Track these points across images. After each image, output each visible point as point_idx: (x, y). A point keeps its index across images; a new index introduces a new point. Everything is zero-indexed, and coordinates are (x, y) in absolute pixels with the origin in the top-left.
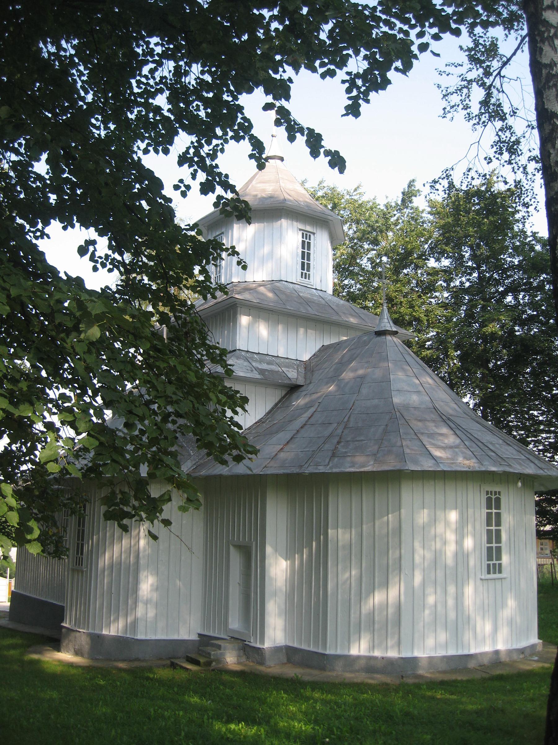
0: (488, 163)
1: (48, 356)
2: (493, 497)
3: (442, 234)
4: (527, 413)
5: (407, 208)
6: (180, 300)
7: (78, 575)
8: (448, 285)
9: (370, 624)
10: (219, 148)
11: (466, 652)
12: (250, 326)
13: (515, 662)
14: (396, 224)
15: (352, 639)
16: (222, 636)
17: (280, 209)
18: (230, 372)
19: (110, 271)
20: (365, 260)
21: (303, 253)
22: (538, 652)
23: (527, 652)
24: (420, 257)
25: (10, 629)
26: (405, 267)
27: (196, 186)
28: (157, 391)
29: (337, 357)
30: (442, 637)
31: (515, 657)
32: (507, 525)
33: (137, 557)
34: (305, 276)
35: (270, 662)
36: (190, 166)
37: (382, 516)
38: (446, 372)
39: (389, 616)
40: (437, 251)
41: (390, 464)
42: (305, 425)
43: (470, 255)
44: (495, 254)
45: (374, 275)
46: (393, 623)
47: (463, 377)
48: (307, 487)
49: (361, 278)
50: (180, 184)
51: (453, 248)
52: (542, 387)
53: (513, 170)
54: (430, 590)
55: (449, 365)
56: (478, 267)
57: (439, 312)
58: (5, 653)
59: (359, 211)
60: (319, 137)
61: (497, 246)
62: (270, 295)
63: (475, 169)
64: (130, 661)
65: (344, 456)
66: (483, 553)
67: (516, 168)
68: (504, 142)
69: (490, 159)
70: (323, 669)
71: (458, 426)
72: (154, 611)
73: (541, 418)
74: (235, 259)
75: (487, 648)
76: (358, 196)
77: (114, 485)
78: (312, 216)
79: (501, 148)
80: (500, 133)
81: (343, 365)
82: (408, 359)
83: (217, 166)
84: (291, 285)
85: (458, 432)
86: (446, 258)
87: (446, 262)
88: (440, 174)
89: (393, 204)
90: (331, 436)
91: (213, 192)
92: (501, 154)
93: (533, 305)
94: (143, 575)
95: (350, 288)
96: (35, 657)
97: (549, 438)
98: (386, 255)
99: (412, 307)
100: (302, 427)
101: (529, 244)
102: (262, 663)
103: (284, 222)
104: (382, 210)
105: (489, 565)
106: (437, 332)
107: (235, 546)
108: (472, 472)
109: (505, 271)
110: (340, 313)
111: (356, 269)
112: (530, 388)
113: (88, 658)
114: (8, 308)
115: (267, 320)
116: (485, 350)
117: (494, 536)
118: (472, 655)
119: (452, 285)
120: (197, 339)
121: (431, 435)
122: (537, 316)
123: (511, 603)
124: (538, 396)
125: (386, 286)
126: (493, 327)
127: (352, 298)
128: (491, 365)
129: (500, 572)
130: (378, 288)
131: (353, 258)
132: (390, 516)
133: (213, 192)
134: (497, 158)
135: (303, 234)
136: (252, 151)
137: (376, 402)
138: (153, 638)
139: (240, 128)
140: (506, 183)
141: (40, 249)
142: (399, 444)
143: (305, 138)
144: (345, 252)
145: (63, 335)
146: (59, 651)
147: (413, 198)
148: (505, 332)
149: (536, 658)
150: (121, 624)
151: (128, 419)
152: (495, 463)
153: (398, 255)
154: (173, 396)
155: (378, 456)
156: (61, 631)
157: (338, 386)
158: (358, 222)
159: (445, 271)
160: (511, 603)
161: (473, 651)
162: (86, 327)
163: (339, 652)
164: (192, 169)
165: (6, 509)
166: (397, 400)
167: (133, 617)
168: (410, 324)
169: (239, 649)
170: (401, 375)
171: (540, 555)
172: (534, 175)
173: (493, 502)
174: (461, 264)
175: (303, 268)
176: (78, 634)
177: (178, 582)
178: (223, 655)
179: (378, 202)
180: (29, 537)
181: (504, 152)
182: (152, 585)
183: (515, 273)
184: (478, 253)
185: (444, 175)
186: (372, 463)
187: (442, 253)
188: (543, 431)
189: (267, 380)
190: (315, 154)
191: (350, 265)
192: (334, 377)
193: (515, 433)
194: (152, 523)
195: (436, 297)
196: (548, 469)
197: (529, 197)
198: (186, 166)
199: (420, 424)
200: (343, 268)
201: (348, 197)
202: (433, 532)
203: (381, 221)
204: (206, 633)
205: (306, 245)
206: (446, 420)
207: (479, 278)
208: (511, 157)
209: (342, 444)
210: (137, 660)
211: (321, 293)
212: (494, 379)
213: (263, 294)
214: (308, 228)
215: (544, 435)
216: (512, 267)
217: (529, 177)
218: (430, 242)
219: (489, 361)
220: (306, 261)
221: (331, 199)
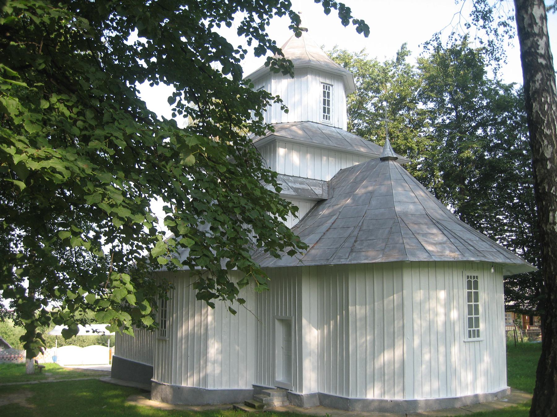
0: (468, 28)
1: (154, 178)
2: (473, 280)
3: (428, 84)
4: (495, 217)
5: (401, 64)
6: (241, 137)
7: (163, 343)
8: (433, 122)
9: (381, 375)
10: (265, 22)
11: (453, 396)
12: (286, 155)
13: (491, 403)
14: (393, 77)
15: (368, 387)
16: (271, 387)
17: (306, 68)
18: (279, 189)
19: (185, 116)
20: (370, 105)
21: (324, 100)
22: (508, 395)
23: (500, 396)
24: (411, 102)
25: (112, 384)
26: (400, 109)
27: (251, 50)
28: (234, 203)
29: (352, 178)
30: (436, 385)
31: (490, 399)
32: (483, 301)
33: (206, 329)
34: (327, 118)
35: (307, 405)
36: (246, 36)
37: (388, 296)
38: (432, 188)
39: (396, 370)
40: (424, 96)
41: (394, 257)
42: (329, 229)
43: (450, 99)
44: (468, 98)
45: (376, 115)
46: (400, 373)
47: (446, 191)
48: (333, 275)
49: (367, 118)
50: (239, 50)
51: (436, 94)
52: (506, 197)
53: (487, 33)
54: (426, 350)
55: (435, 182)
56: (456, 108)
57: (427, 142)
58: (111, 401)
59: (364, 68)
60: (348, 10)
61: (469, 92)
62: (300, 132)
63: (457, 33)
64: (203, 406)
65: (360, 251)
66: (465, 322)
67: (489, 31)
68: (480, 11)
69: (469, 25)
70: (347, 409)
71: (445, 228)
72: (220, 369)
73: (505, 221)
74: (279, 105)
75: (469, 393)
76: (363, 56)
77: (201, 274)
78: (329, 73)
79: (477, 16)
80: (476, 5)
81: (356, 184)
82: (406, 178)
83: (267, 35)
84: (316, 125)
85: (445, 232)
86: (431, 102)
87: (431, 105)
88: (431, 37)
89: (390, 62)
90: (349, 236)
91: (264, 55)
92: (478, 21)
93: (498, 136)
94: (211, 342)
95: (359, 126)
96: (132, 403)
97: (512, 236)
98: (385, 100)
99: (406, 139)
100: (327, 231)
101: (494, 89)
102: (301, 406)
103: (309, 77)
104: (382, 67)
105: (470, 331)
106: (426, 158)
107: (278, 319)
108: (456, 262)
109: (476, 110)
110: (353, 145)
111: (363, 112)
112: (497, 198)
113: (172, 404)
114: (125, 143)
115: (299, 151)
116: (462, 170)
117: (473, 310)
118: (458, 398)
119: (436, 122)
120: (254, 165)
121: (425, 235)
122: (502, 144)
123: (487, 358)
124: (503, 205)
125: (389, 124)
126: (468, 153)
127: (361, 133)
128: (466, 182)
129: (478, 336)
130: (380, 125)
131: (360, 103)
132: (395, 295)
133: (264, 55)
134: (475, 24)
135: (324, 86)
136: (292, 23)
137: (382, 210)
138: (220, 388)
139: (282, 6)
140: (481, 42)
141: (142, 99)
142: (401, 241)
143: (338, 11)
144: (355, 99)
145: (163, 163)
146: (150, 399)
147: (405, 57)
148: (476, 157)
149: (506, 400)
150: (196, 378)
151: (213, 224)
152: (473, 255)
153: (395, 100)
154: (246, 206)
155: (386, 250)
156: (151, 384)
157: (354, 200)
158: (363, 76)
159: (431, 112)
160: (487, 358)
161: (458, 395)
162: (184, 156)
163: (359, 397)
164: (248, 38)
165: (127, 293)
166: (398, 209)
167: (204, 373)
168: (405, 152)
169: (284, 396)
170: (400, 189)
171: (507, 324)
172: (503, 36)
173: (473, 284)
174: (443, 106)
175: (324, 112)
176: (164, 387)
177: (237, 347)
178: (272, 400)
179: (378, 61)
180: (143, 313)
181: (480, 19)
182: (217, 350)
183: (484, 112)
184: (456, 97)
185: (434, 38)
186: (381, 256)
187: (429, 98)
188: (507, 231)
189: (302, 195)
190: (345, 22)
191: (358, 109)
192: (350, 193)
193: (486, 233)
194: (232, 301)
195: (424, 131)
196: (513, 259)
197: (500, 53)
198: (244, 35)
199: (416, 227)
200: (353, 112)
201: (356, 57)
202: (427, 307)
203: (382, 75)
204: (258, 384)
205: (327, 94)
206: (436, 223)
207: (457, 116)
208: (485, 22)
209: (358, 242)
210: (208, 404)
211: (338, 130)
212: (470, 192)
213: (295, 132)
214: (328, 81)
215: (508, 234)
216: (482, 108)
217: (499, 38)
218: (419, 90)
219: (464, 179)
220: (326, 106)
221: (343, 59)
